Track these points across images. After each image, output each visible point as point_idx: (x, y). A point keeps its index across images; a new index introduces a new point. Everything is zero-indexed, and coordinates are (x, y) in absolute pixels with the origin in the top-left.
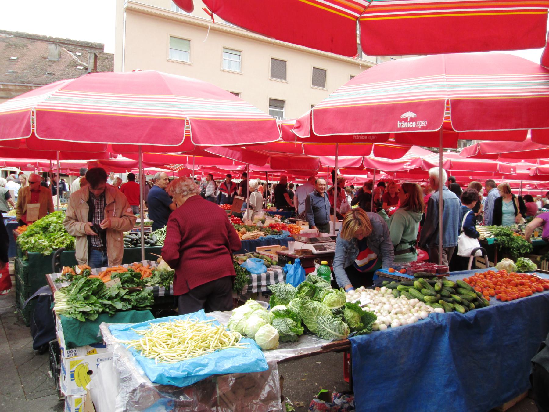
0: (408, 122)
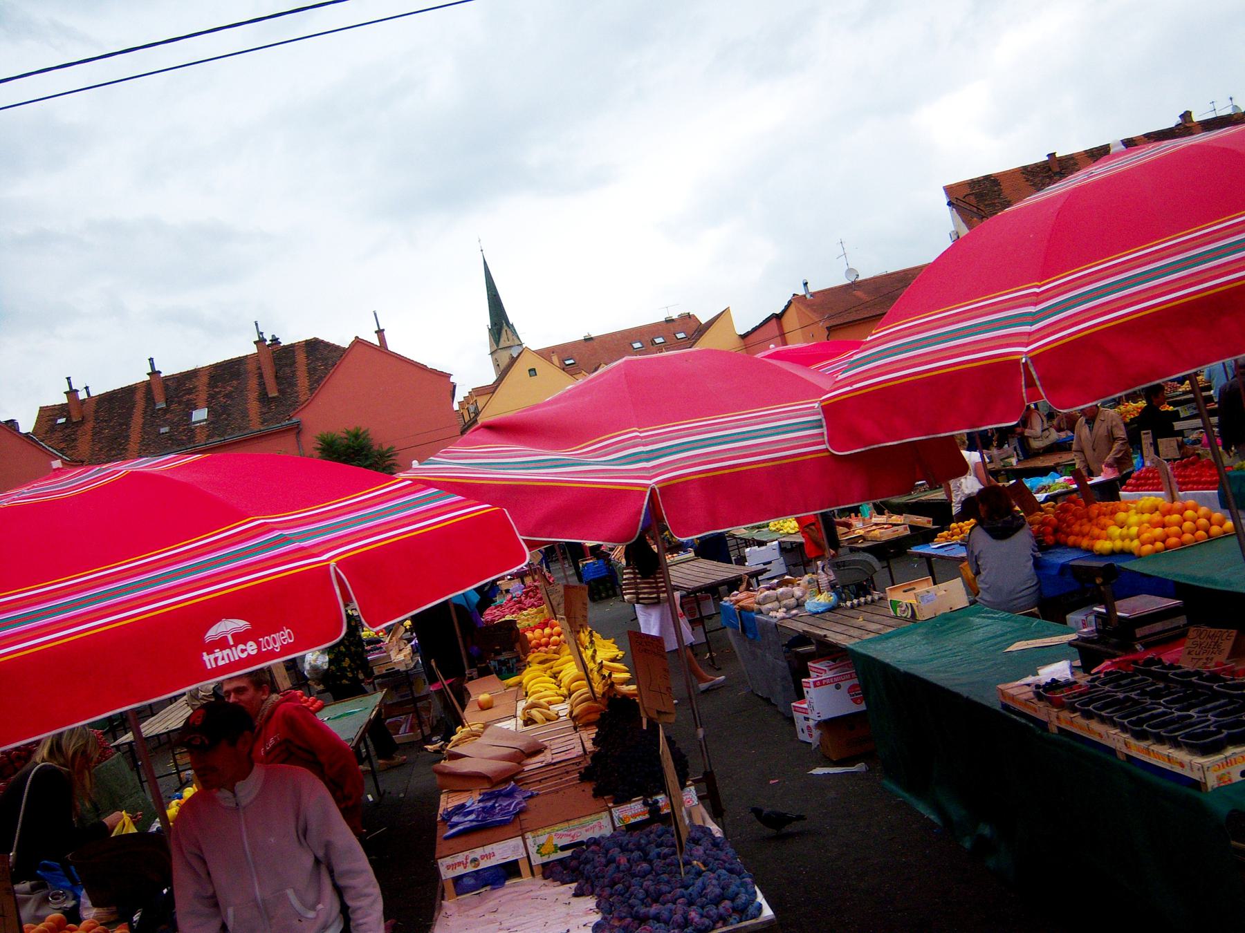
0: (230, 647)
